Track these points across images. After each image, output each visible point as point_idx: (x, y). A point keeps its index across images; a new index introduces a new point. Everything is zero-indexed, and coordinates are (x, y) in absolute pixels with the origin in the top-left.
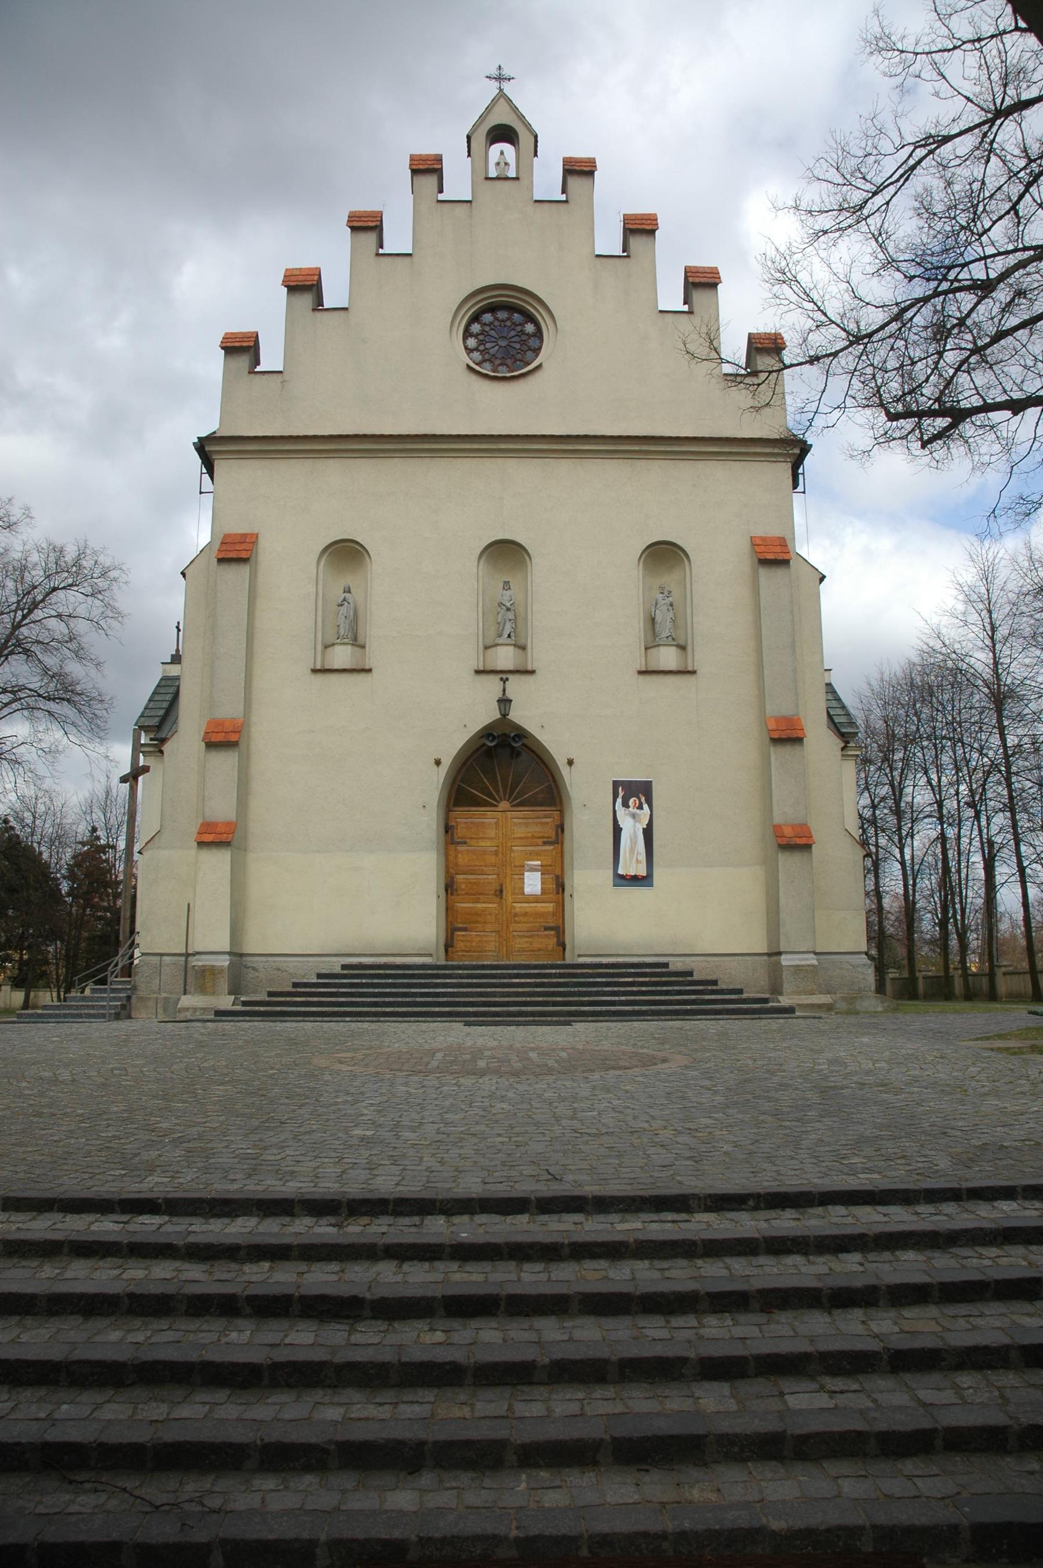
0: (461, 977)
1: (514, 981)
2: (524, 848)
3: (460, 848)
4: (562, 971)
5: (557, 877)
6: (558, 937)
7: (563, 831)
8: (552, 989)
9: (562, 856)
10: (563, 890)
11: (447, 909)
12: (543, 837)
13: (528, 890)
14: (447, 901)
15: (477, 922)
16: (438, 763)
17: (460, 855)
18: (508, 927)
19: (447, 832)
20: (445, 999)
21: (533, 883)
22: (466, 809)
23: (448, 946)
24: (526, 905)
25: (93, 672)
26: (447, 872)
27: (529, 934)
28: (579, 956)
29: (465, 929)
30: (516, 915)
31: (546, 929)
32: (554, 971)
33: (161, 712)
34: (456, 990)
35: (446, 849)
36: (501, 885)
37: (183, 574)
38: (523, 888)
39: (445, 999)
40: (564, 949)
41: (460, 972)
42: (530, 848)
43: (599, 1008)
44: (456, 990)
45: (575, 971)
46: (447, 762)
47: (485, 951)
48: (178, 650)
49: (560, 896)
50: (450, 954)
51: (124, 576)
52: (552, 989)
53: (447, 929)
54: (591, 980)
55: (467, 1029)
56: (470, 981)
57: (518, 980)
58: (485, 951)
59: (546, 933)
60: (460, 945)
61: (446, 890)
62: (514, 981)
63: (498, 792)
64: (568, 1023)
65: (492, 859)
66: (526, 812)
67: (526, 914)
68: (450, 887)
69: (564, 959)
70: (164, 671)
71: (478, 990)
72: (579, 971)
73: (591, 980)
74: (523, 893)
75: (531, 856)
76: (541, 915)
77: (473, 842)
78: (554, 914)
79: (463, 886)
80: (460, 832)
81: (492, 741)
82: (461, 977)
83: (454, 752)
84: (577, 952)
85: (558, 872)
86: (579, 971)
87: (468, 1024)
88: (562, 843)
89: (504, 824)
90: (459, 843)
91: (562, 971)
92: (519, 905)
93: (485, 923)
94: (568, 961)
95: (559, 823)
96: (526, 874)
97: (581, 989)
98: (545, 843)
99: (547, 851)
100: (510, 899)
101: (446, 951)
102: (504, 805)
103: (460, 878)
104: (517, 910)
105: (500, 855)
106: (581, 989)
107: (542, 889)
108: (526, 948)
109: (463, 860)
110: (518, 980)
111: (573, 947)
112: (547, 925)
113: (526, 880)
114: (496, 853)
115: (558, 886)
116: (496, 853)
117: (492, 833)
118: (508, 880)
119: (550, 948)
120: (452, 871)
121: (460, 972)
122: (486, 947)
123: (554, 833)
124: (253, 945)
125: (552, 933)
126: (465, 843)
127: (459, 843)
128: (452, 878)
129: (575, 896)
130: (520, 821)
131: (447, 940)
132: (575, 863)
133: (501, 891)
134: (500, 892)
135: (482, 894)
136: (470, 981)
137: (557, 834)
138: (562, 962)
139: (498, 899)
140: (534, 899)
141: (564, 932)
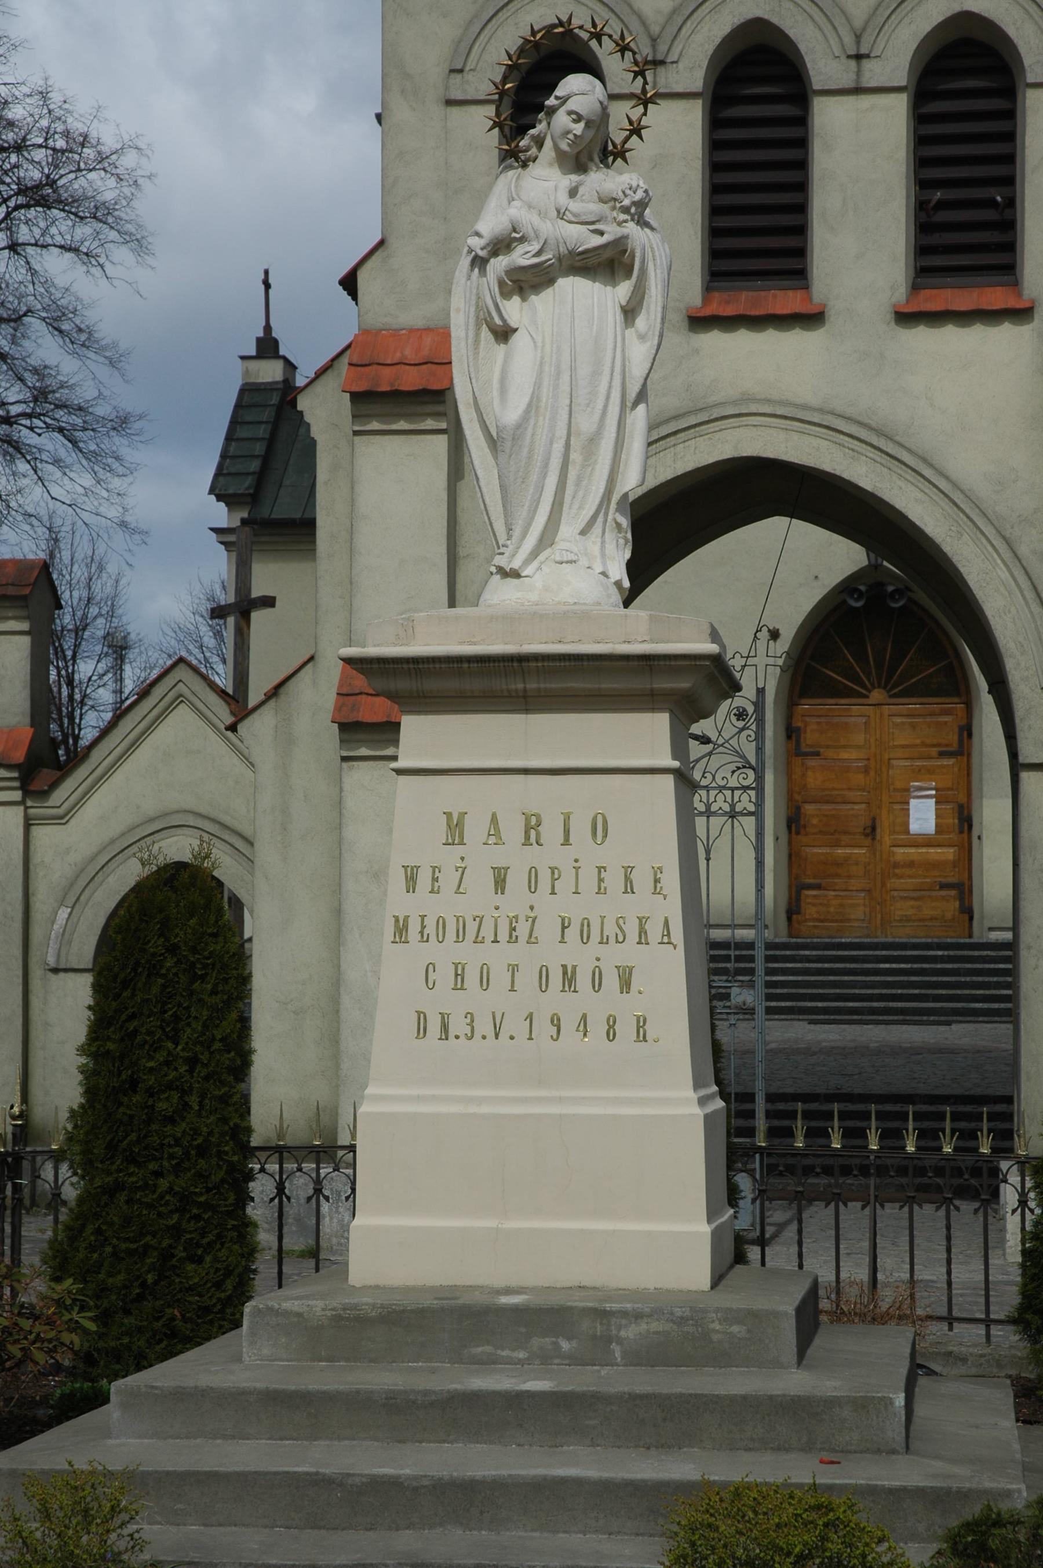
0: (808, 959)
1: (882, 966)
2: (907, 763)
3: (812, 762)
4: (952, 953)
5: (961, 807)
6: (961, 899)
7: (970, 735)
8: (935, 979)
9: (969, 774)
10: (970, 827)
11: (790, 856)
12: (939, 745)
13: (914, 827)
14: (790, 843)
15: (837, 876)
16: (775, 635)
17: (810, 773)
18: (884, 884)
19: (789, 737)
20: (785, 991)
21: (923, 815)
22: (819, 701)
23: (793, 911)
24: (913, 850)
25: (103, 372)
26: (790, 798)
27: (918, 894)
28: (991, 929)
29: (818, 887)
30: (896, 865)
31: (943, 886)
32: (940, 953)
33: (255, 466)
34: (800, 978)
35: (789, 764)
36: (874, 820)
37: (350, 283)
38: (907, 824)
39: (785, 991)
40: (971, 919)
41: (807, 953)
42: (918, 763)
43: (996, 1006)
44: (800, 978)
45: (971, 953)
46: (788, 634)
47: (849, 920)
48: (268, 328)
49: (965, 836)
50: (795, 925)
51: (144, 161)
52: (935, 979)
53: (790, 887)
54: (992, 966)
55: (812, 1027)
56: (820, 965)
57: (887, 966)
58: (849, 920)
59: (943, 893)
60: (810, 911)
61: (789, 827)
62: (882, 966)
63: (868, 675)
64: (948, 1023)
65: (859, 779)
66: (913, 705)
67: (911, 864)
68: (794, 823)
69: (970, 936)
70: (246, 373)
71: (832, 978)
72: (976, 953)
73: (992, 966)
74: (907, 832)
75: (918, 773)
76: (936, 865)
77: (831, 753)
78: (955, 864)
79: (815, 821)
80: (810, 737)
81: (857, 600)
82: (808, 959)
83: (800, 619)
84: (987, 924)
85: (962, 798)
86: (976, 953)
87: (811, 1022)
88: (969, 755)
89: (877, 726)
90: (807, 754)
91: (952, 953)
92: (902, 850)
93: (849, 877)
94: (975, 940)
95: (964, 722)
96: (913, 802)
97: (975, 979)
98: (942, 754)
99: (943, 766)
100: (887, 840)
101: (789, 919)
102: (877, 695)
103: (809, 809)
104: (898, 858)
105: (872, 773)
106: (975, 979)
107: (937, 825)
108: (913, 916)
109: (815, 779)
110: (887, 966)
111: (982, 918)
112: (943, 880)
113: (911, 812)
114: (866, 770)
115: (961, 820)
116: (866, 770)
117: (859, 738)
118: (884, 812)
119: (949, 915)
120: (797, 797)
121: (807, 953)
122: (849, 913)
123: (956, 738)
124: (90, 966)
125: (953, 893)
126: (818, 754)
127: (807, 754)
128: (798, 808)
129: (984, 838)
130: (904, 720)
131: (790, 903)
132: (985, 788)
133: (874, 829)
134: (871, 831)
135: (845, 833)
136: (820, 965)
137: (961, 742)
138: (967, 940)
139: (868, 841)
140: (926, 841)
141: (971, 892)
